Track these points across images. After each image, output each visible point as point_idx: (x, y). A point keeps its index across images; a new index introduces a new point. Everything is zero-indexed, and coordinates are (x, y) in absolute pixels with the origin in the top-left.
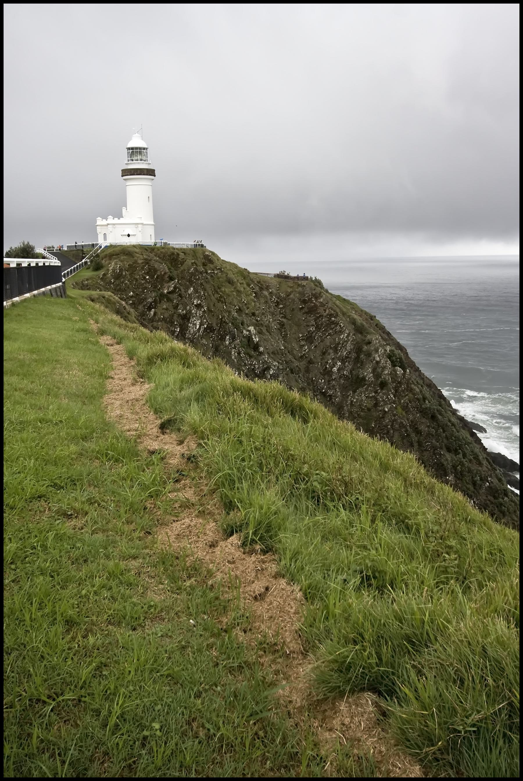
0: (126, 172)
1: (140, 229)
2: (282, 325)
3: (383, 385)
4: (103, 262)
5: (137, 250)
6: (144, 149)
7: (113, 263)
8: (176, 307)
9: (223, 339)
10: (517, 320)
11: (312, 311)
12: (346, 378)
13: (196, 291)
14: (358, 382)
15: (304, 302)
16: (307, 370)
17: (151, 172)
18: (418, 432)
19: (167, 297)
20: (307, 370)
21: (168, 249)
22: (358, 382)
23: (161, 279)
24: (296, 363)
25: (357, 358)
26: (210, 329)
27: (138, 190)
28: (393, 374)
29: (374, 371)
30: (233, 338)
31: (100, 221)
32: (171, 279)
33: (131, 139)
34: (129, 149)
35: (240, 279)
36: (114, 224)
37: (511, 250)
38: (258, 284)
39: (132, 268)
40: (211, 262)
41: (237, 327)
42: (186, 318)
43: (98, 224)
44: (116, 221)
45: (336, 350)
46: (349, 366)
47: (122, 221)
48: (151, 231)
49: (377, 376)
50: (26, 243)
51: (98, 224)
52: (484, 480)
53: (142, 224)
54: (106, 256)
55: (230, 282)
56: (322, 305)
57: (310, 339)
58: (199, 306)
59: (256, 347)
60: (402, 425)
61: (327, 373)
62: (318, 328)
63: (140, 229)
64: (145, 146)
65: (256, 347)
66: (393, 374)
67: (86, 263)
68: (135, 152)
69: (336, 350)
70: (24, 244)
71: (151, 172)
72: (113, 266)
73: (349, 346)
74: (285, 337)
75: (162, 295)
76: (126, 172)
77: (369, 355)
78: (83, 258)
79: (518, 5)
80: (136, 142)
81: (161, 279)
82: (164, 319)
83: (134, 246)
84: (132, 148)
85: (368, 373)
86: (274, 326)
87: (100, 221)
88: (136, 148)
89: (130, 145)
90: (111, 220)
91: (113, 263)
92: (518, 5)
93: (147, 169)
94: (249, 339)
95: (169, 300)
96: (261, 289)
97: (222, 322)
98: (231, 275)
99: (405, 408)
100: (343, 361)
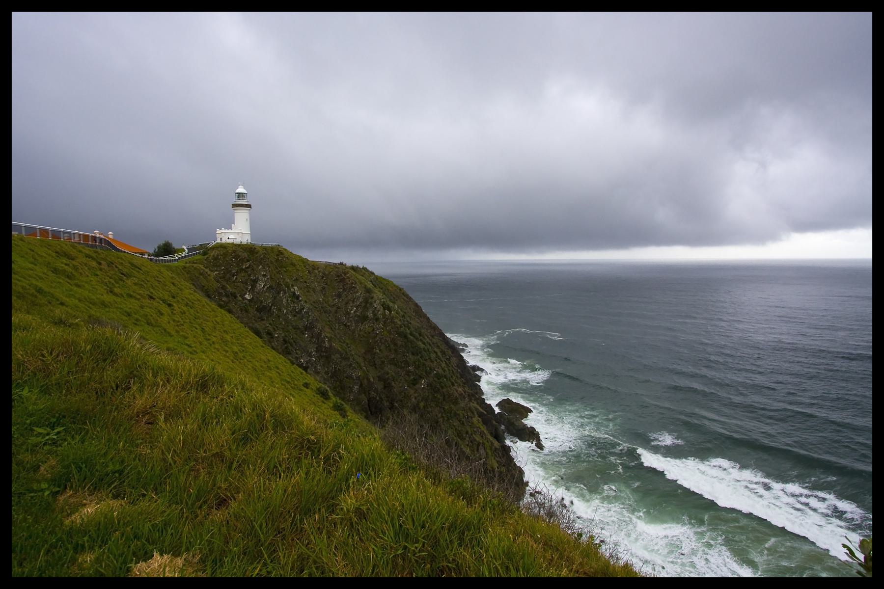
0: (235, 206)
2: (324, 288)
3: (377, 320)
8: (250, 275)
9: (279, 293)
11: (342, 280)
12: (359, 316)
13: (263, 267)
14: (364, 318)
15: (338, 276)
16: (336, 312)
17: (249, 206)
18: (396, 344)
19: (245, 270)
20: (336, 312)
22: (364, 318)
23: (243, 261)
24: (329, 308)
25: (365, 306)
26: (271, 287)
28: (384, 315)
29: (373, 312)
30: (285, 293)
31: (218, 231)
32: (248, 261)
35: (300, 263)
38: (313, 267)
39: (225, 255)
40: (282, 253)
41: (288, 287)
42: (255, 281)
44: (226, 231)
45: (353, 302)
46: (360, 310)
49: (375, 315)
52: (432, 369)
55: (293, 265)
56: (348, 278)
57: (339, 296)
58: (264, 276)
59: (298, 298)
60: (386, 341)
61: (348, 313)
62: (344, 290)
65: (298, 298)
66: (384, 315)
68: (240, 195)
69: (353, 302)
71: (249, 206)
72: (213, 253)
73: (361, 300)
74: (324, 295)
75: (242, 269)
76: (235, 206)
77: (371, 304)
79: (870, 14)
80: (241, 190)
81: (243, 261)
82: (242, 282)
85: (370, 314)
86: (318, 289)
87: (218, 231)
90: (223, 230)
92: (871, 13)
94: (294, 293)
95: (246, 272)
96: (314, 269)
97: (279, 284)
98: (294, 261)
99: (389, 332)
100: (357, 308)
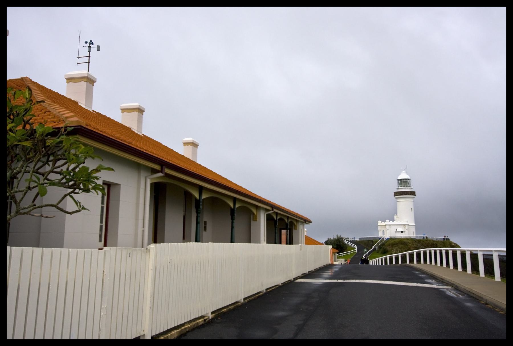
0: (396, 194)
1: (407, 228)
4: (388, 248)
5: (410, 242)
6: (408, 179)
7: (395, 250)
10: (118, 338)
17: (413, 193)
21: (430, 241)
27: (405, 205)
31: (380, 223)
33: (400, 174)
34: (399, 180)
36: (390, 225)
37: (505, 249)
43: (379, 224)
47: (395, 223)
48: (413, 229)
50: (339, 236)
51: (379, 224)
53: (408, 225)
54: (389, 245)
63: (407, 228)
64: (409, 178)
67: (375, 248)
68: (403, 182)
70: (337, 236)
78: (373, 245)
79: (9, 9)
80: (404, 176)
83: (407, 239)
84: (401, 180)
87: (380, 223)
88: (404, 179)
89: (400, 178)
90: (388, 222)
91: (395, 250)
92: (9, 9)
93: (411, 192)
